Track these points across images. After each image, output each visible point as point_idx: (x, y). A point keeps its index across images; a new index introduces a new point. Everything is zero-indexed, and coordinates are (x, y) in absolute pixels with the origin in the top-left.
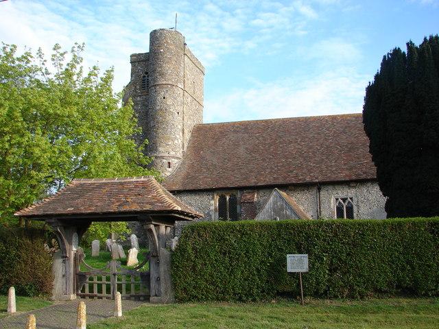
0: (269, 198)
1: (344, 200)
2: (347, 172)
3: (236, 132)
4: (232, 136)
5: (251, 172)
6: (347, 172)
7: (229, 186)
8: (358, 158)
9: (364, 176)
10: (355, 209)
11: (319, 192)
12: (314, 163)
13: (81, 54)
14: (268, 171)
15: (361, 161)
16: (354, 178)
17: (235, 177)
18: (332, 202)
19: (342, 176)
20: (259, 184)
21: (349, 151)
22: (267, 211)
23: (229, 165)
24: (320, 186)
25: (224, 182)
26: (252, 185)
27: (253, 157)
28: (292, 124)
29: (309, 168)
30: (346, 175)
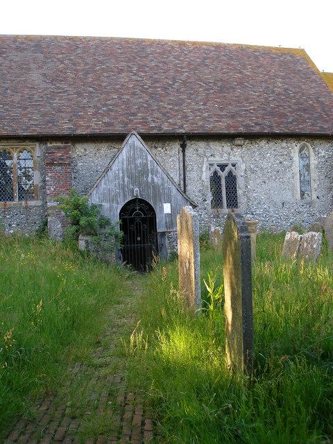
0: (120, 150)
1: (223, 167)
2: (230, 122)
3: (18, 49)
4: (17, 57)
5: (59, 111)
6: (230, 122)
7: (20, 133)
8: (239, 102)
9: (257, 129)
10: (240, 182)
11: (184, 151)
12: (169, 104)
13: (74, 227)
14: (90, 111)
15: (244, 106)
16: (242, 130)
17: (30, 119)
18: (204, 169)
19: (221, 127)
20: (79, 132)
21: (221, 91)
22: (117, 177)
23: (17, 98)
24: (184, 139)
25: (11, 126)
26: (66, 133)
27: (59, 88)
28: (118, 46)
29: (164, 111)
30: (229, 126)
